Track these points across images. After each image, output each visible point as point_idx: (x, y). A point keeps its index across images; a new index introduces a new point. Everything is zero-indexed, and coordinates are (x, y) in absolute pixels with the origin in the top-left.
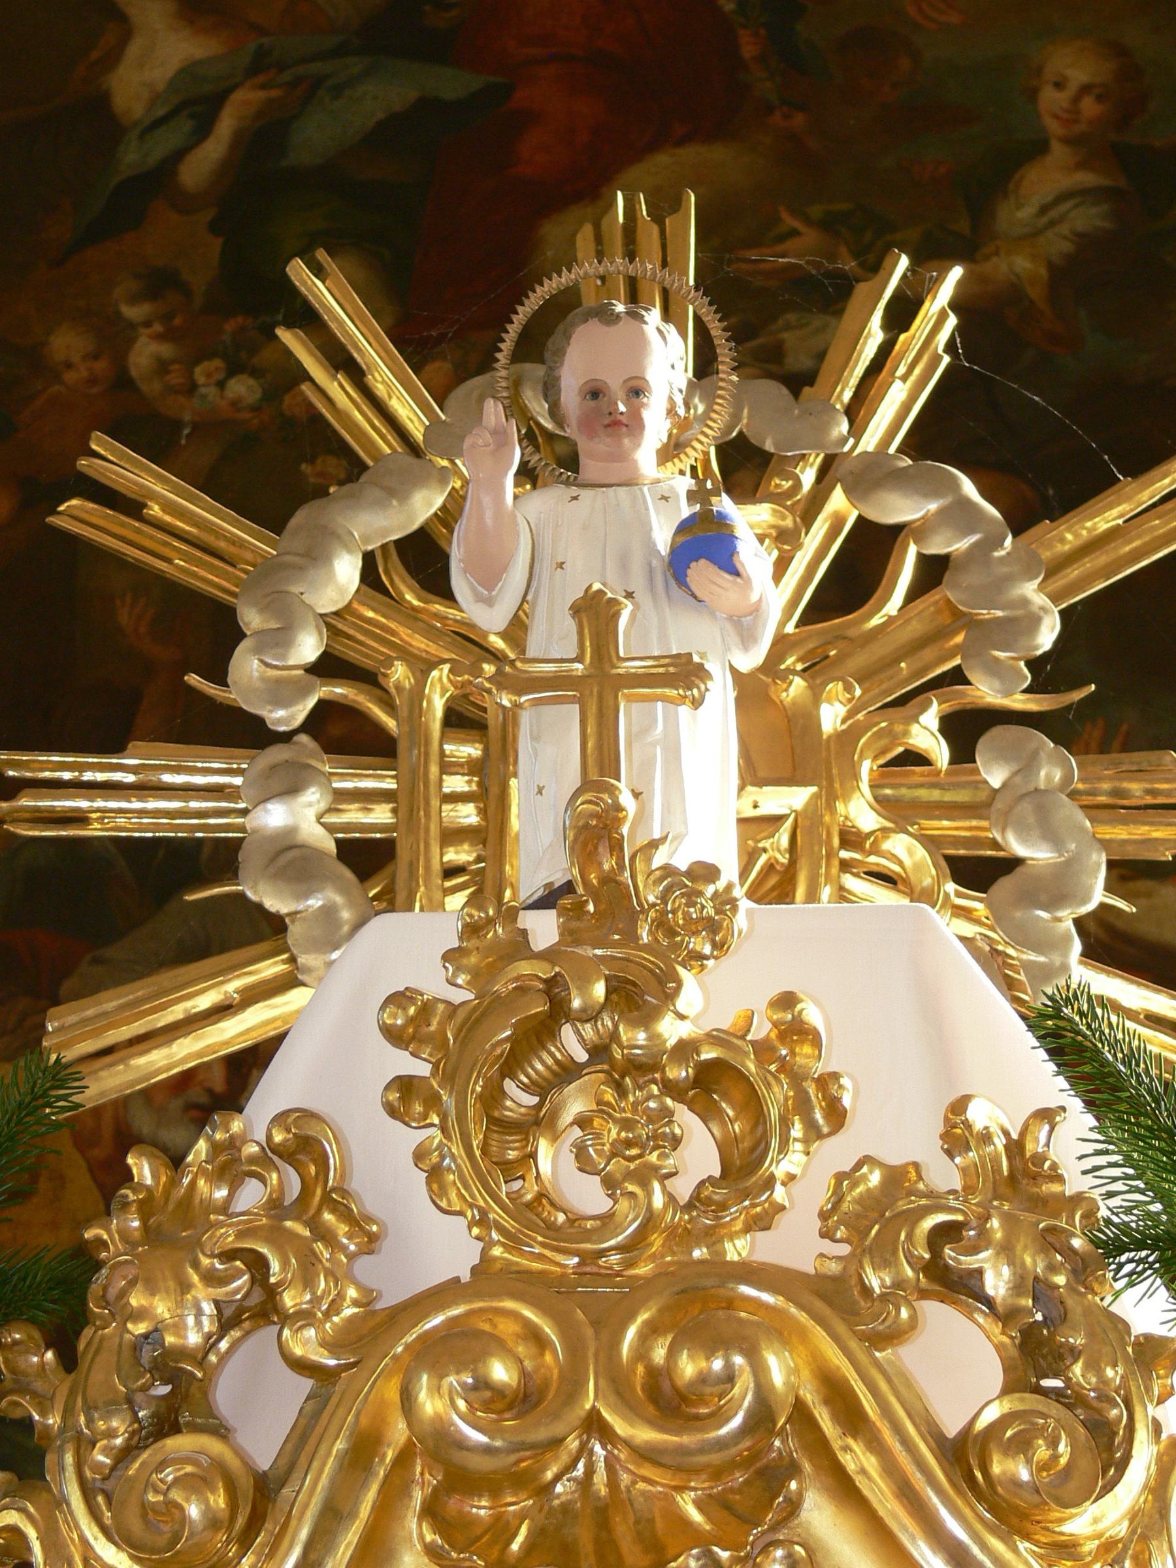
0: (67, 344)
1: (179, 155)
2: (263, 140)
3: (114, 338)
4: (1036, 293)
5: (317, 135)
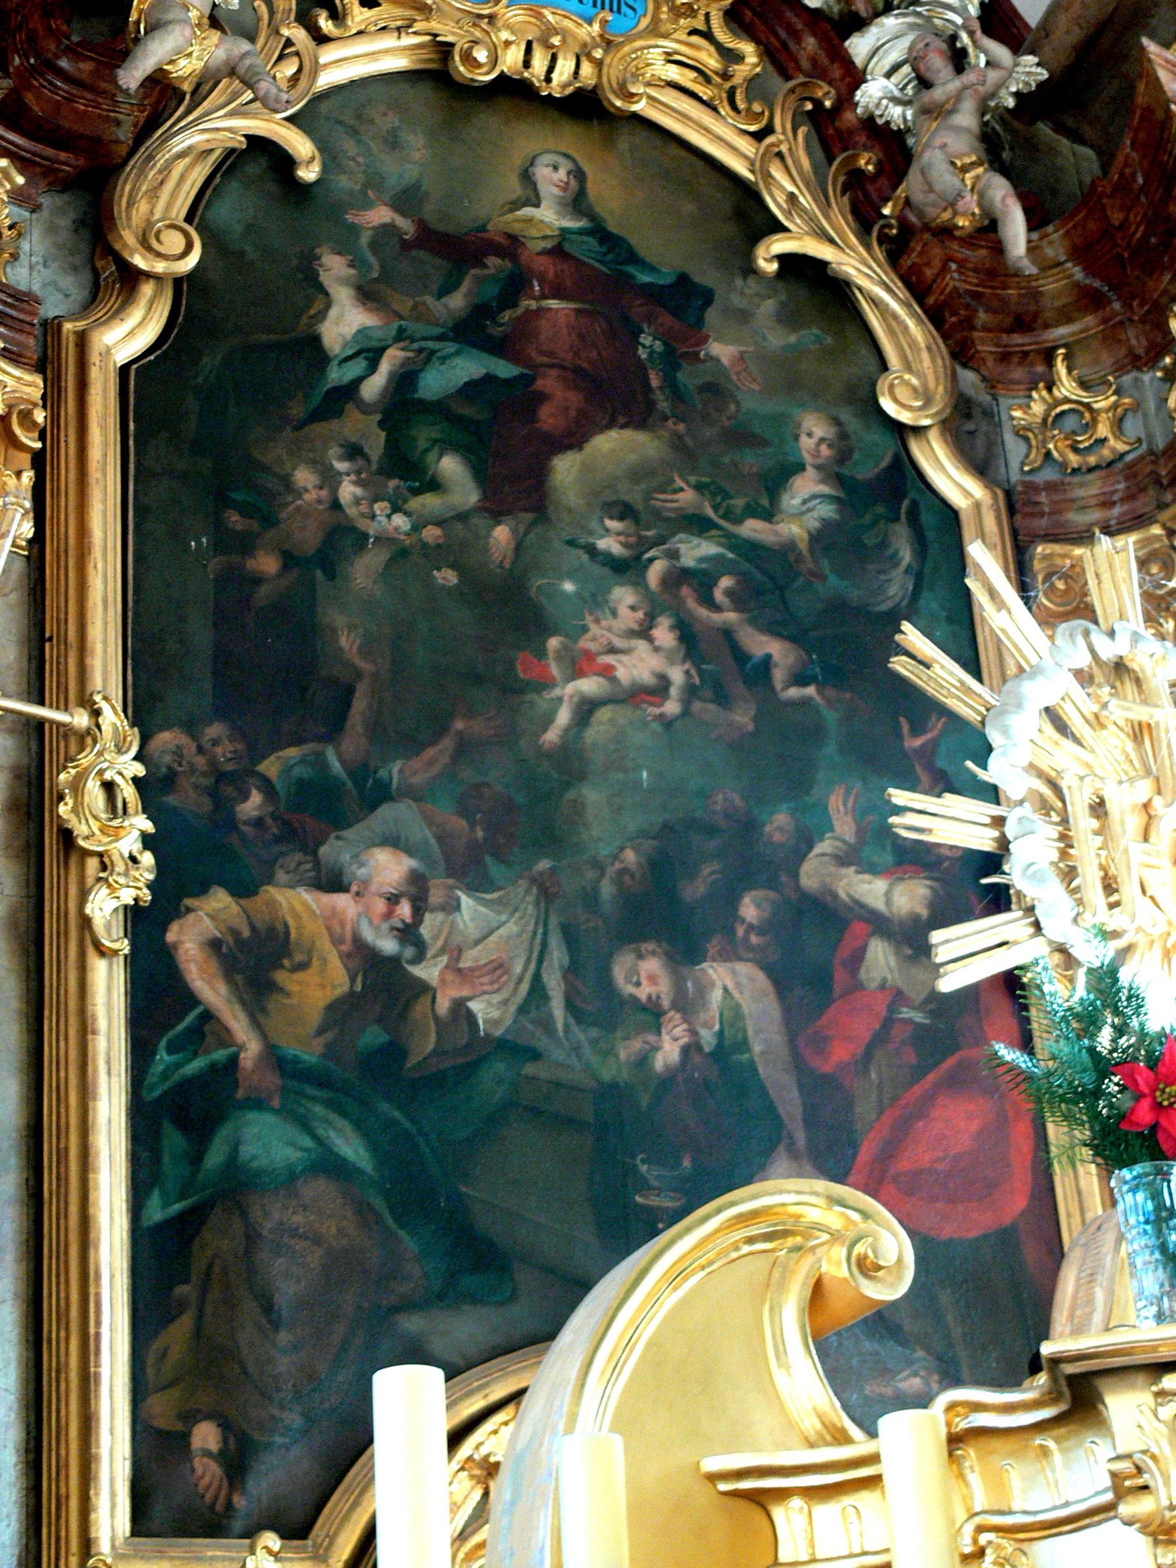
0: (304, 477)
1: (360, 380)
2: (404, 380)
3: (330, 479)
4: (803, 546)
5: (436, 382)
